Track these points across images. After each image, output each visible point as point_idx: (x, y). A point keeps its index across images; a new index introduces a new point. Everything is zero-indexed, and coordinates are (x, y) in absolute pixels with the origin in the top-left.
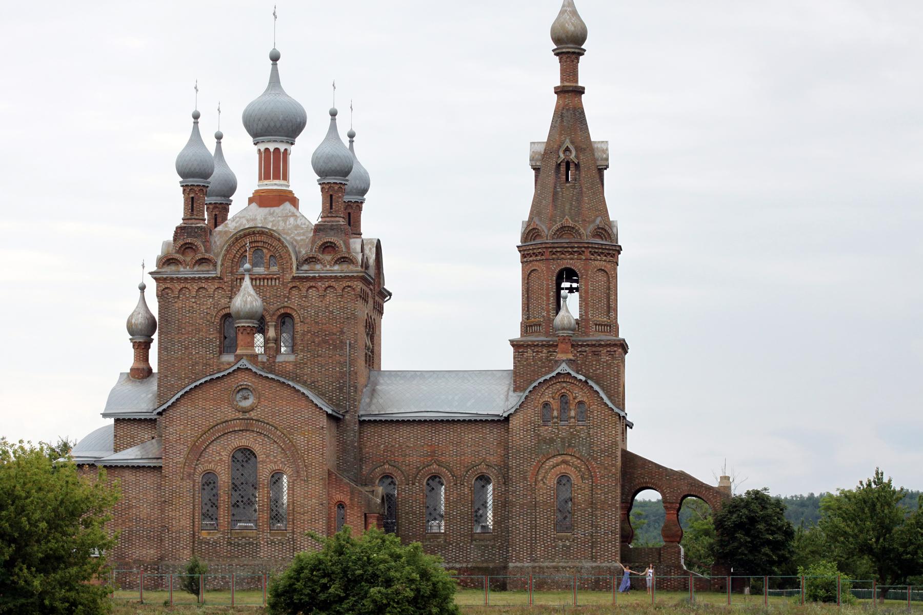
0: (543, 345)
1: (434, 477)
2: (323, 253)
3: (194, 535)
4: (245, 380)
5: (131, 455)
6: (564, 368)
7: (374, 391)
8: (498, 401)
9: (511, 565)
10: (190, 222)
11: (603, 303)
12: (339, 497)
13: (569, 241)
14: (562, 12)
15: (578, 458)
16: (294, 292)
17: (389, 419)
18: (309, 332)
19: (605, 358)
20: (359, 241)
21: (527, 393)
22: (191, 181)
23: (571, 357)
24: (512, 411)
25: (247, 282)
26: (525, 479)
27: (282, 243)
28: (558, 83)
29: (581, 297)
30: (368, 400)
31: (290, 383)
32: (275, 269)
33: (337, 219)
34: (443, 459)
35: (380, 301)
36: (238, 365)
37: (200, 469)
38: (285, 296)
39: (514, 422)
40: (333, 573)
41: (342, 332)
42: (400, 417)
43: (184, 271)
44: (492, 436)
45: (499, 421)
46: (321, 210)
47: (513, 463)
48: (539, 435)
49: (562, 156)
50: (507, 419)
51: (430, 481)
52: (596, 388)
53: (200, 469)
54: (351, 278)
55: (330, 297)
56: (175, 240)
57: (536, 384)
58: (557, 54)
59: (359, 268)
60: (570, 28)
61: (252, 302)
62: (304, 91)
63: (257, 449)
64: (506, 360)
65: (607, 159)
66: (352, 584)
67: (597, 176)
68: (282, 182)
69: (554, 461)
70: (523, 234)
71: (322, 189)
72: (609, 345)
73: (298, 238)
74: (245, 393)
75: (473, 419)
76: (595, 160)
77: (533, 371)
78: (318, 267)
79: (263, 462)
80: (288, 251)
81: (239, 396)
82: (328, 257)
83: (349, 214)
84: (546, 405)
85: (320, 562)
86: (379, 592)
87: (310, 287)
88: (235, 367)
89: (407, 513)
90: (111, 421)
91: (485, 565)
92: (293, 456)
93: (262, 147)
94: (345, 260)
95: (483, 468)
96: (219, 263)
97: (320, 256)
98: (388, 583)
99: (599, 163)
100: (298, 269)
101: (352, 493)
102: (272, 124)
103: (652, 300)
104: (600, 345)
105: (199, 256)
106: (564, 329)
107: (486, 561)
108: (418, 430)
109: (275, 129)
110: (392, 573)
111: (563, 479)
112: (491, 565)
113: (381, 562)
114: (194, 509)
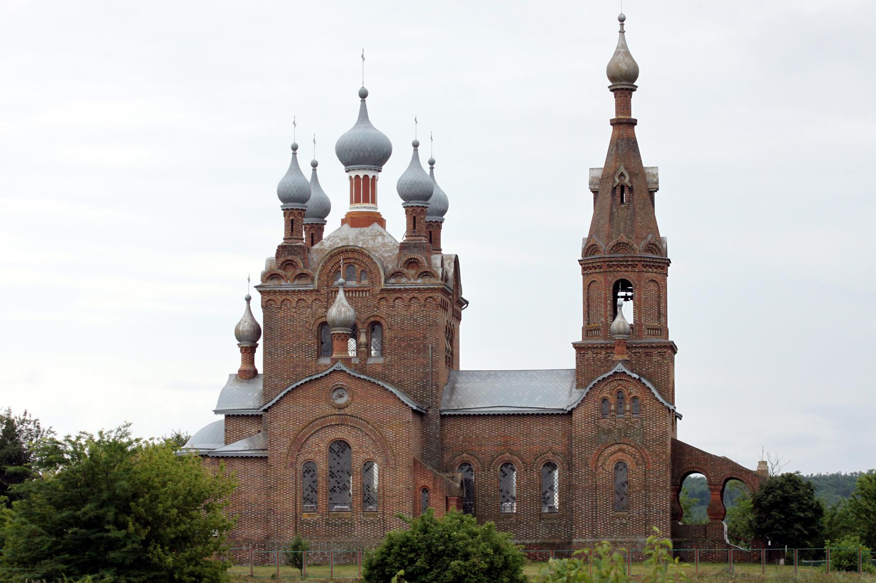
0: (601, 347)
1: (506, 464)
2: (408, 268)
3: (296, 516)
4: (340, 380)
5: (240, 447)
6: (620, 367)
7: (453, 390)
8: (563, 397)
9: (574, 540)
10: (290, 241)
11: (655, 309)
12: (423, 482)
13: (625, 252)
14: (617, 53)
15: (633, 447)
16: (383, 302)
17: (467, 413)
18: (395, 337)
19: (656, 358)
21: (588, 390)
22: (290, 205)
23: (627, 358)
24: (575, 406)
25: (341, 294)
26: (587, 465)
27: (372, 260)
28: (613, 116)
29: (634, 304)
30: (448, 397)
31: (380, 383)
32: (365, 282)
33: (420, 238)
34: (514, 448)
35: (459, 309)
37: (301, 459)
38: (375, 306)
39: (576, 416)
40: (419, 549)
41: (425, 338)
42: (472, 412)
43: (285, 285)
44: (557, 427)
45: (563, 414)
46: (405, 230)
47: (576, 451)
48: (598, 427)
49: (617, 180)
50: (570, 413)
51: (504, 468)
52: (649, 385)
53: (301, 459)
54: (433, 290)
55: (415, 306)
56: (277, 257)
57: (595, 382)
58: (612, 91)
59: (440, 281)
60: (624, 67)
61: (345, 312)
62: (386, 124)
63: (351, 440)
64: (569, 361)
65: (657, 183)
66: (435, 558)
67: (649, 198)
68: (371, 205)
69: (612, 449)
70: (584, 249)
71: (407, 212)
72: (660, 347)
73: (386, 255)
74: (340, 392)
75: (540, 413)
76: (647, 184)
77: (593, 370)
78: (404, 280)
79: (357, 452)
80: (376, 266)
81: (335, 394)
82: (412, 272)
83: (430, 232)
84: (604, 400)
85: (408, 539)
86: (459, 565)
87: (397, 298)
88: (331, 370)
89: (483, 496)
90: (222, 417)
91: (552, 541)
92: (383, 447)
93: (353, 174)
94: (427, 274)
95: (550, 456)
96: (316, 277)
97: (405, 271)
98: (466, 556)
99: (650, 186)
100: (385, 282)
101: (435, 479)
102: (362, 154)
104: (652, 347)
105: (299, 272)
106: (619, 333)
107: (553, 537)
108: (492, 423)
109: (365, 158)
110: (469, 549)
111: (620, 465)
112: (557, 541)
113: (460, 540)
114: (296, 494)
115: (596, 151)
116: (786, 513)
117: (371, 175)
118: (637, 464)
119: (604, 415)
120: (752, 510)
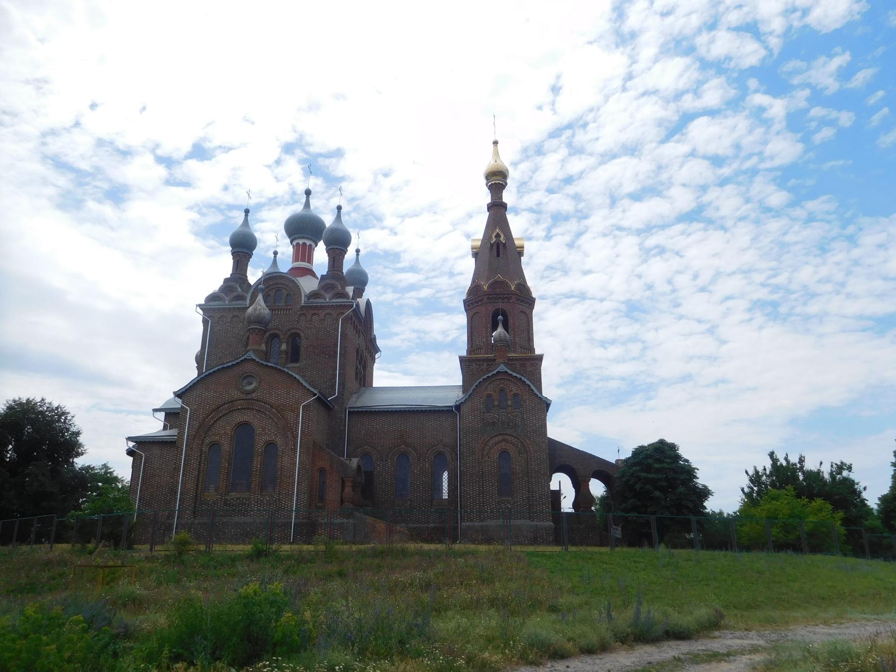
4: (249, 367)
6: (502, 368)
8: (452, 398)
13: (499, 300)
16: (303, 318)
36: (245, 357)
39: (464, 409)
53: (208, 440)
57: (481, 380)
69: (497, 439)
74: (250, 379)
84: (489, 396)
88: (243, 358)
90: (162, 415)
93: (295, 243)
103: (557, 335)
105: (235, 294)
111: (504, 454)
115: (478, 226)
116: (807, 512)
117: (308, 242)
118: (519, 453)
119: (488, 411)
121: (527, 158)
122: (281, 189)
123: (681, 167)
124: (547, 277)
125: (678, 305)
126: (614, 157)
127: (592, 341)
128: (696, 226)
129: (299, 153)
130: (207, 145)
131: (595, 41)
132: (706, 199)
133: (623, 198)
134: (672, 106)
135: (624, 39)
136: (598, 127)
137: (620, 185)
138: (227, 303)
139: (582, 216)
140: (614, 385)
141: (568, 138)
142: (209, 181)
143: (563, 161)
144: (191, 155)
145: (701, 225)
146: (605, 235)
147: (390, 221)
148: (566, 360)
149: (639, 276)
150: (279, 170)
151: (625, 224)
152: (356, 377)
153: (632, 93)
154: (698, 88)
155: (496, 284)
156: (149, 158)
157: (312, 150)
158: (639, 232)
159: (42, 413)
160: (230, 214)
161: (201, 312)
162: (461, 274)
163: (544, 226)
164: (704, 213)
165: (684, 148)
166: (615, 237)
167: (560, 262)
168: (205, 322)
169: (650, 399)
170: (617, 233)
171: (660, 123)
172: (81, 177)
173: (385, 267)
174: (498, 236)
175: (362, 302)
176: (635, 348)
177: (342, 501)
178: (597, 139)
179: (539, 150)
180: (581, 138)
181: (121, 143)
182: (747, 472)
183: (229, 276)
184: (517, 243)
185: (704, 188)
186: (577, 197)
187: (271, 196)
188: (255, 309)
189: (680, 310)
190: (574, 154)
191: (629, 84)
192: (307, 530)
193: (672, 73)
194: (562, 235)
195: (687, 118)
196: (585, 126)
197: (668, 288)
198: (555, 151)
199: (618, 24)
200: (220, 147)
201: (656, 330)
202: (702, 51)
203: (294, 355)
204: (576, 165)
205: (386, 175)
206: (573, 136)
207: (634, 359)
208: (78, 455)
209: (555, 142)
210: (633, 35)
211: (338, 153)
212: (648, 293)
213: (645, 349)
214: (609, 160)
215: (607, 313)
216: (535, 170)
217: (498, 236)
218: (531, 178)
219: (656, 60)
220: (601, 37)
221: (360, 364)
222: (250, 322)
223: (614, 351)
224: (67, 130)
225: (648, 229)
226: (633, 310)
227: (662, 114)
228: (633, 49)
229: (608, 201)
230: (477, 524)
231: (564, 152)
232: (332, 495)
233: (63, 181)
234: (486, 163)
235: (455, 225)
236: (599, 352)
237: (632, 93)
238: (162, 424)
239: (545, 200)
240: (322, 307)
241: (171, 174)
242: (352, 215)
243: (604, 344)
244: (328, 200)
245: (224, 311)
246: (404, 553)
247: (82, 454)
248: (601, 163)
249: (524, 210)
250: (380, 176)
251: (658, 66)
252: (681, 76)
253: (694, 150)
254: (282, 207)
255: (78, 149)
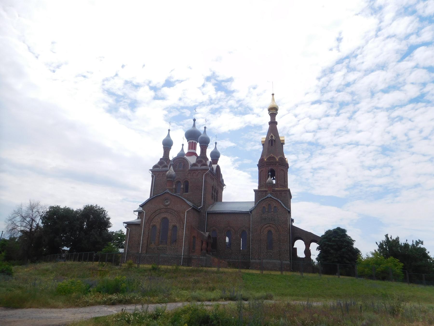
2: (198, 163)
6: (269, 195)
8: (247, 208)
13: (273, 165)
20: (216, 165)
37: (151, 224)
39: (253, 213)
53: (151, 224)
63: (169, 218)
69: (266, 225)
74: (167, 200)
84: (264, 207)
90: (137, 213)
105: (164, 165)
111: (270, 232)
116: (403, 261)
120: (373, 254)
121: (325, 75)
122: (205, 98)
123: (411, 73)
124: (338, 135)
125: (411, 147)
126: (372, 71)
127: (363, 167)
128: (420, 104)
129: (213, 81)
130: (172, 80)
131: (359, 13)
132: (426, 90)
133: (378, 92)
134: (404, 42)
135: (376, 10)
136: (363, 57)
137: (376, 86)
138: (160, 169)
139: (356, 103)
140: (375, 189)
141: (347, 63)
142: (173, 96)
143: (345, 75)
144: (164, 86)
145: (424, 104)
146: (368, 112)
147: (256, 111)
148: (349, 177)
149: (389, 133)
150: (204, 89)
151: (380, 105)
152: (212, 198)
153: (381, 38)
154: (418, 31)
155: (270, 158)
156: (147, 88)
157: (219, 79)
158: (387, 110)
159: (96, 210)
160: (182, 111)
161: (151, 172)
162: (293, 135)
163: (335, 109)
164: (425, 98)
165: (411, 64)
166: (374, 112)
167: (345, 127)
168: (152, 176)
169: (397, 196)
170: (375, 110)
171: (397, 52)
172: (119, 98)
173: (255, 133)
174: (272, 137)
175: (214, 166)
176: (387, 170)
177: (202, 250)
178: (363, 63)
179: (331, 70)
180: (354, 63)
181: (135, 82)
182: (376, 243)
183: (162, 157)
184: (281, 139)
185: (424, 85)
186: (352, 93)
187: (201, 101)
188: (169, 173)
189: (413, 150)
190: (350, 71)
191: (379, 33)
192: (188, 261)
193: (404, 25)
194: (345, 113)
195: (412, 48)
196: (356, 56)
197: (405, 138)
198: (340, 71)
199: (372, 3)
200: (177, 80)
201: (399, 160)
202: (420, 12)
203: (186, 189)
204: (351, 77)
205: (254, 88)
206: (349, 62)
207: (387, 175)
208: (110, 227)
209: (340, 66)
210: (381, 8)
211: (230, 80)
212: (394, 141)
213: (393, 170)
214: (370, 73)
215: (371, 152)
216: (329, 81)
217: (272, 137)
218: (328, 85)
219: (394, 20)
220: (363, 11)
221: (214, 192)
222: (167, 178)
223: (375, 172)
224: (113, 78)
225: (393, 108)
226: (385, 150)
227: (398, 47)
228: (381, 15)
229: (370, 94)
230: (257, 261)
231: (344, 71)
232: (198, 247)
233: (111, 100)
234: (269, 103)
235: (289, 111)
236: (367, 172)
237: (381, 38)
238: (137, 217)
239: (336, 96)
240: (197, 170)
241: (156, 95)
242: (239, 108)
243: (370, 168)
244: (227, 102)
245: (159, 172)
246: (202, 271)
247: (111, 227)
248: (365, 75)
249: (324, 101)
250: (251, 89)
251: (395, 23)
252: (408, 26)
253: (418, 64)
254: (206, 106)
255: (117, 85)
